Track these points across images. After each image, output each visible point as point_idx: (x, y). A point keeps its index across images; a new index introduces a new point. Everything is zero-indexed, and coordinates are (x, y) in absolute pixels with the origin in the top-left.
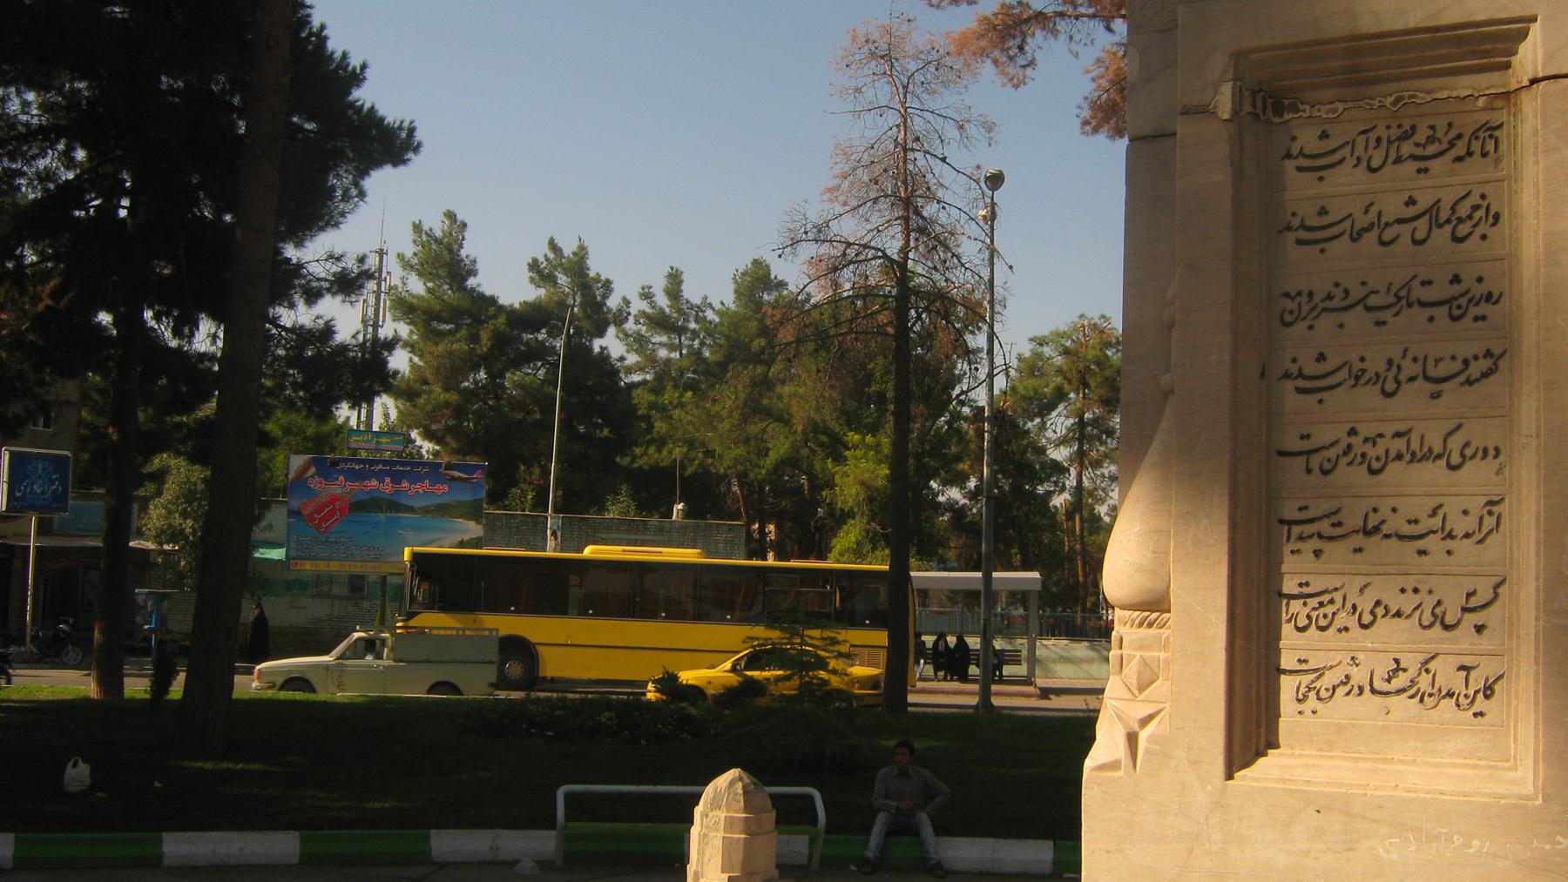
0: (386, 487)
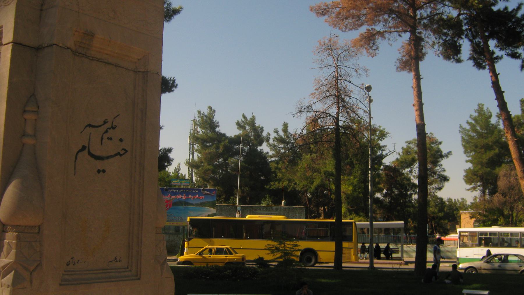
0: (184, 197)
